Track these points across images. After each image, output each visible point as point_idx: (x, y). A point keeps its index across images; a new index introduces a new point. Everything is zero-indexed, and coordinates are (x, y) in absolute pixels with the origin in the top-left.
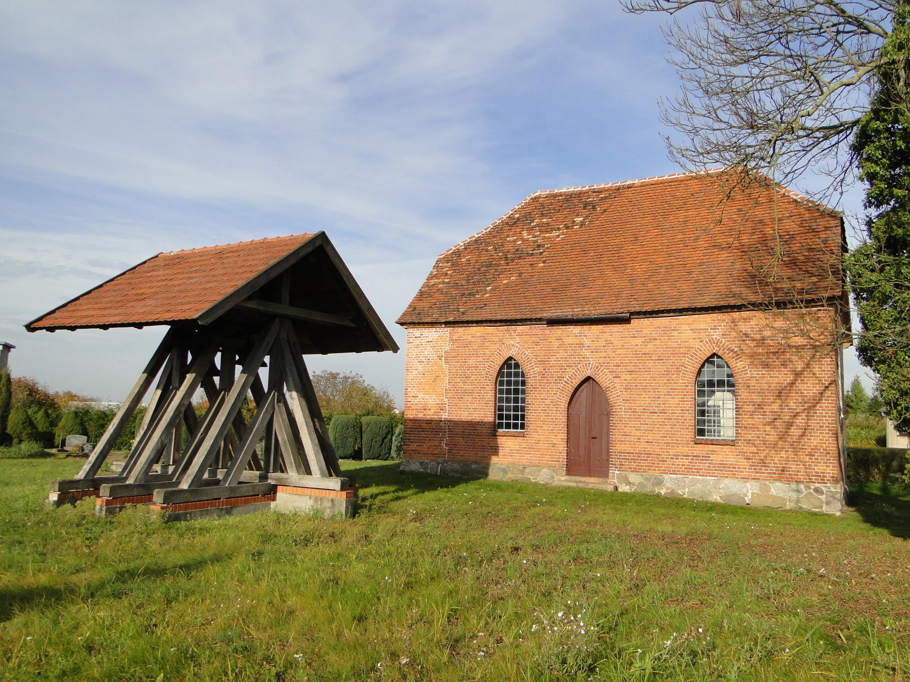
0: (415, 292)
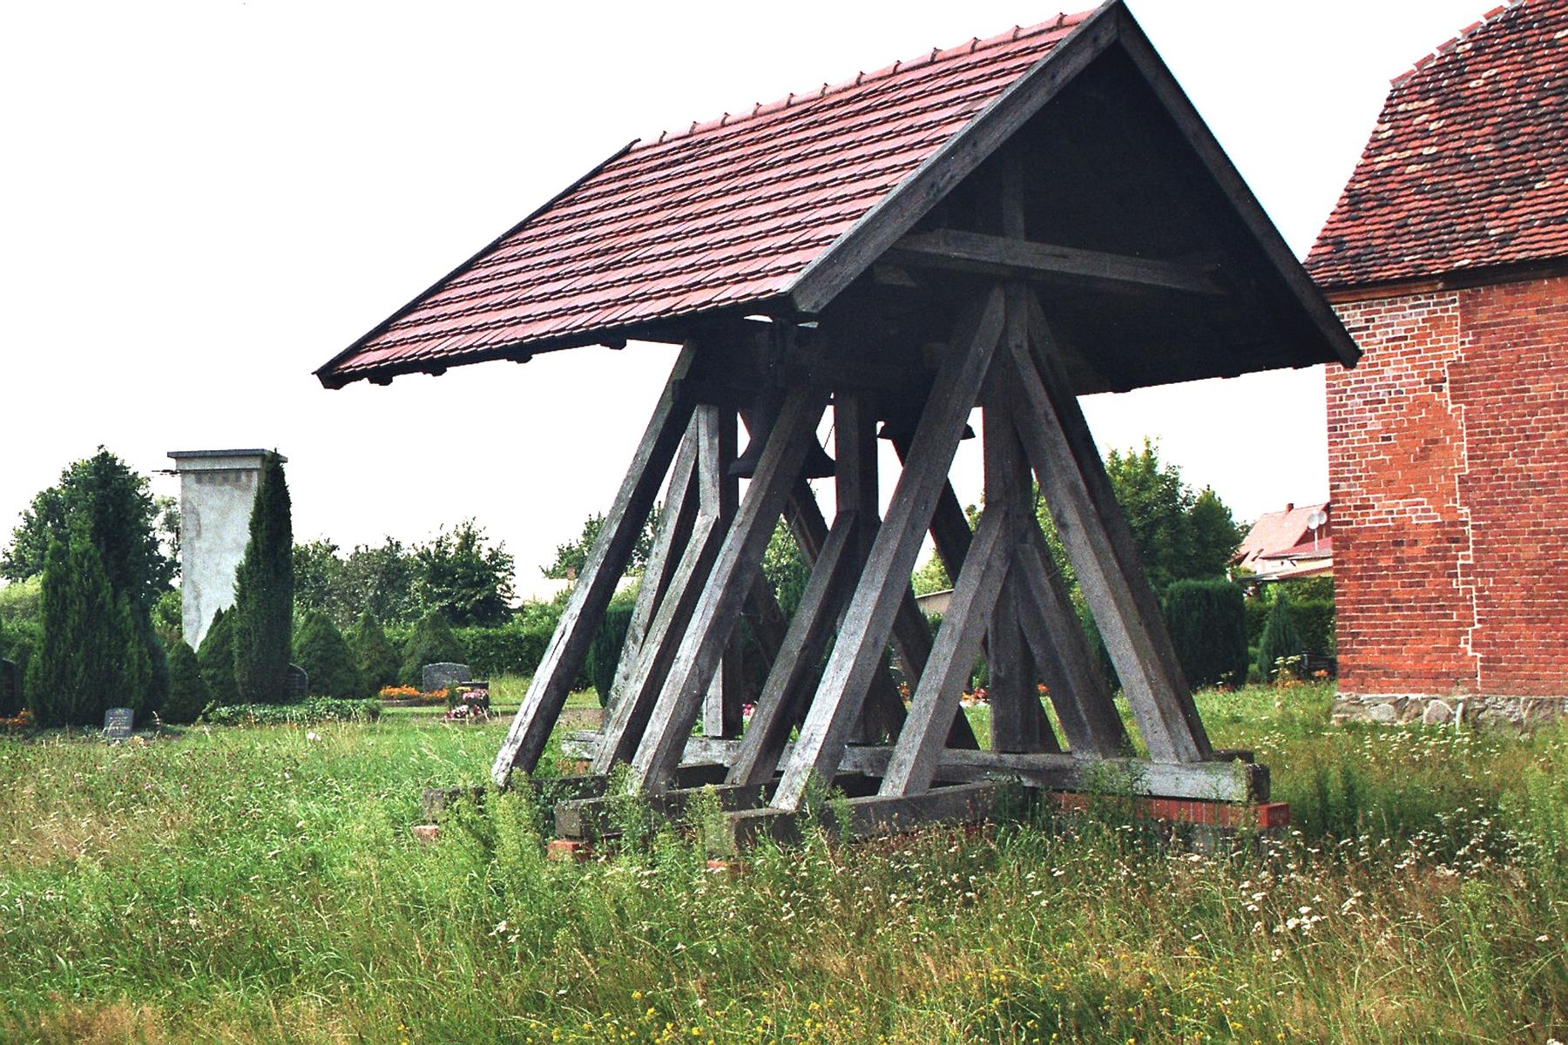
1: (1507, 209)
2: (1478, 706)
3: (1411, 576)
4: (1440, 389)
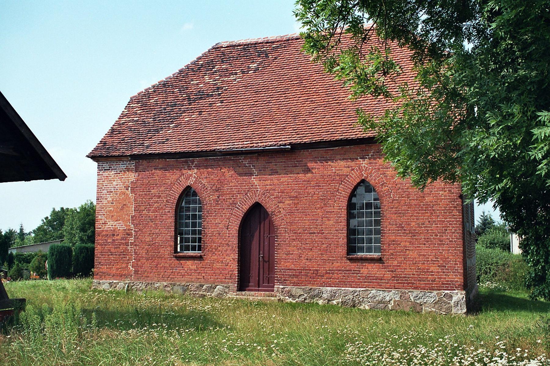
0: (106, 129)
1: (151, 138)
2: (132, 284)
3: (117, 245)
4: (128, 189)
